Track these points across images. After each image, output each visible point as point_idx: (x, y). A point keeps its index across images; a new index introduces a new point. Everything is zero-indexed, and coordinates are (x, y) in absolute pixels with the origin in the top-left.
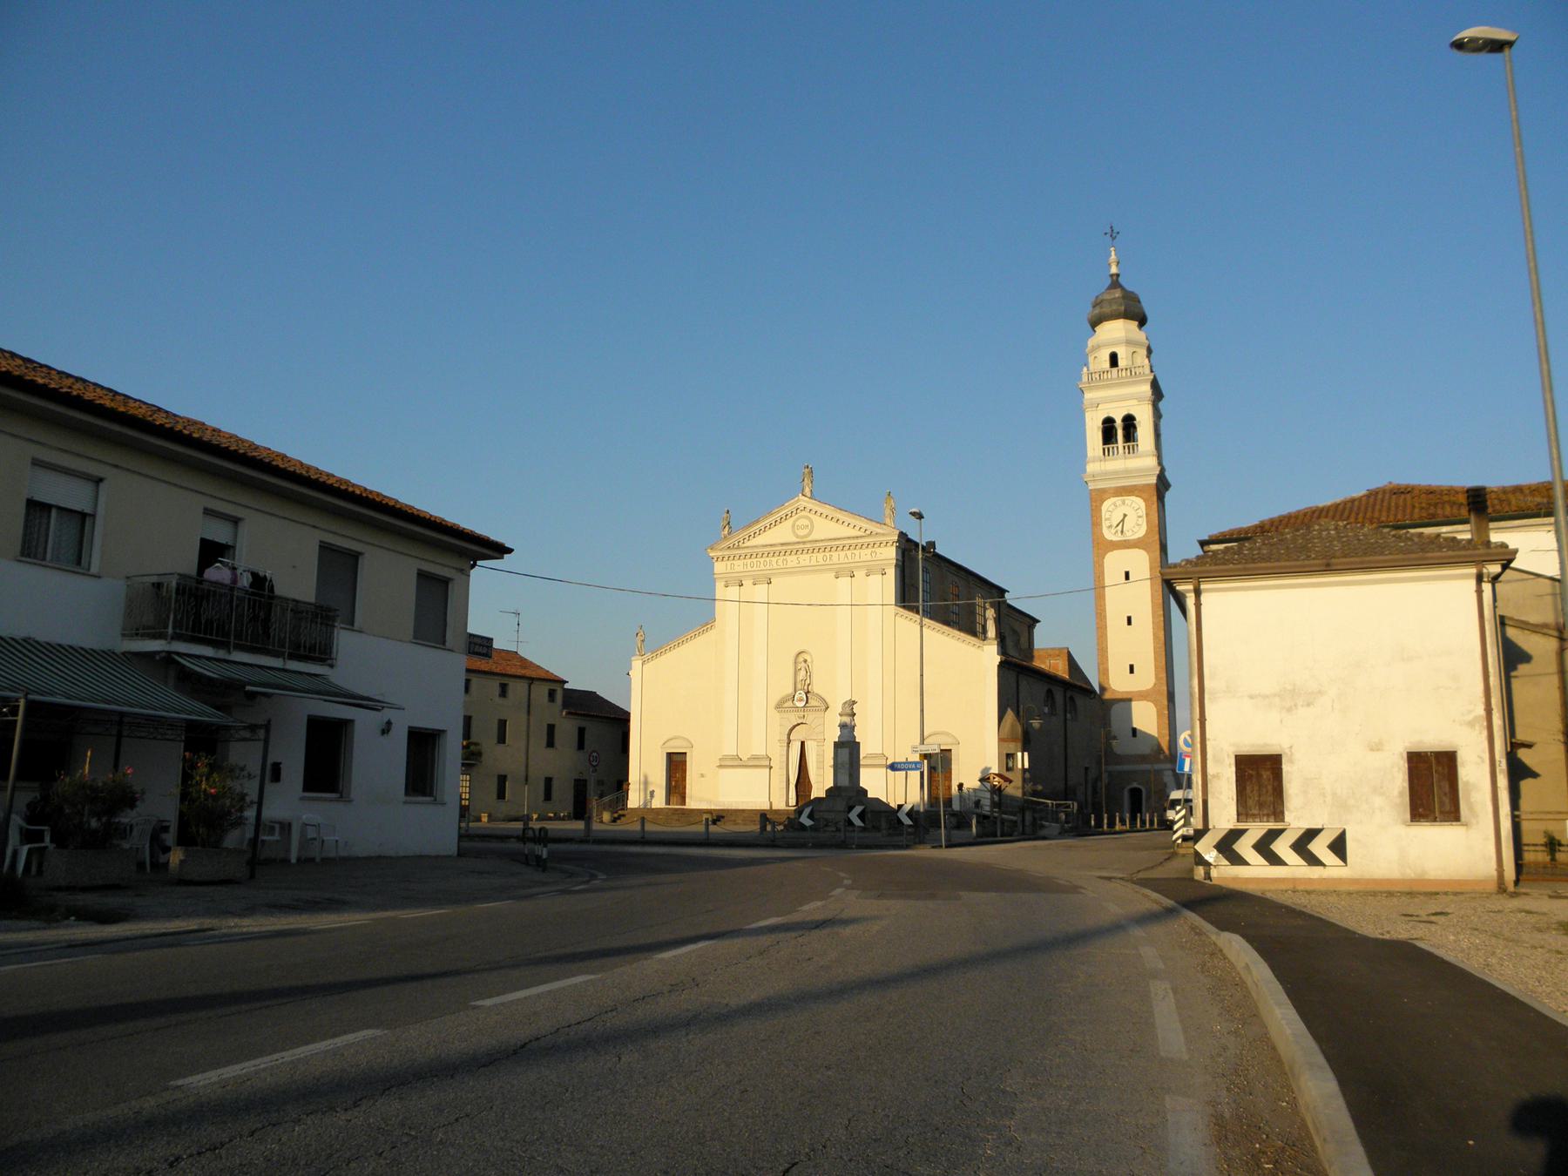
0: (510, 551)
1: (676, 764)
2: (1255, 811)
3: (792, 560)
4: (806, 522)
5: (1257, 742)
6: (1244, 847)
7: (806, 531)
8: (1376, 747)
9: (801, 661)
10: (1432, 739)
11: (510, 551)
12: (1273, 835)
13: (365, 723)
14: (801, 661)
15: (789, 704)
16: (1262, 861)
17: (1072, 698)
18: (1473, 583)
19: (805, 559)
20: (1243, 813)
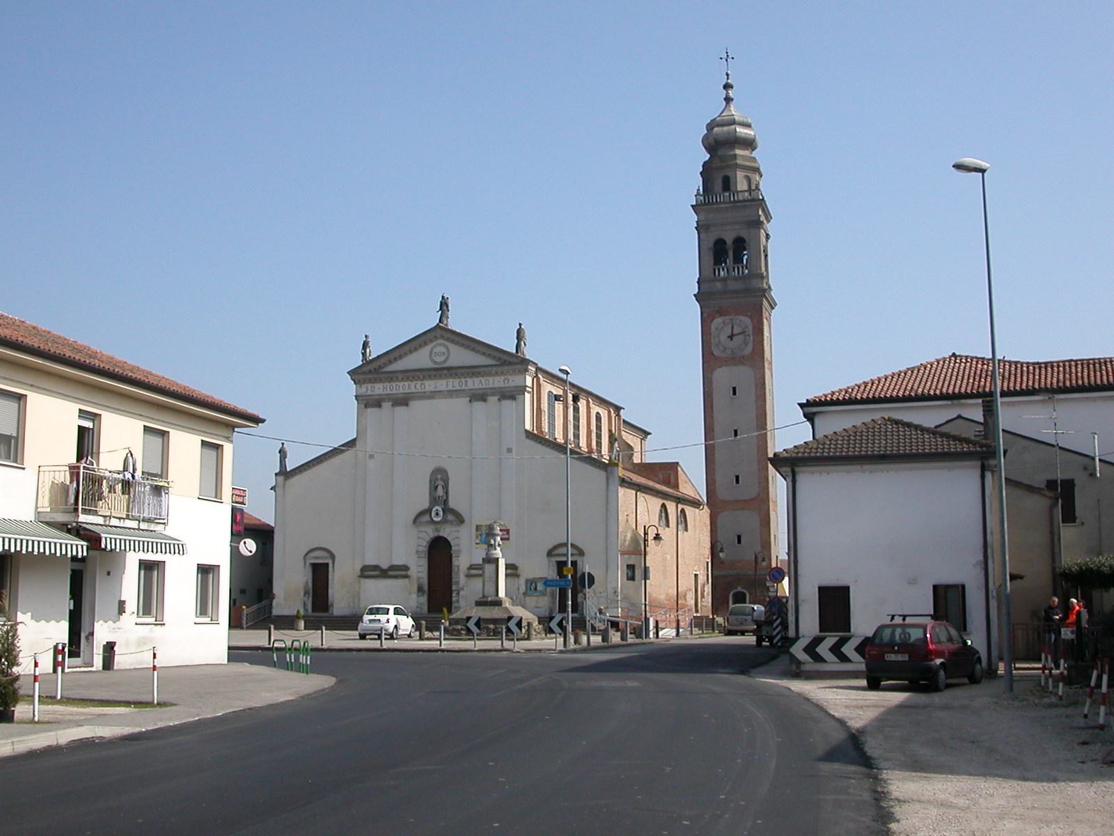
0: (263, 421)
1: (320, 573)
2: (1085, 362)
3: (430, 385)
4: (443, 349)
5: (831, 580)
6: (823, 649)
7: (443, 358)
8: (913, 582)
9: (439, 479)
10: (948, 577)
11: (263, 421)
12: (843, 641)
13: (171, 561)
14: (439, 479)
15: (426, 518)
16: (836, 659)
17: (683, 511)
18: (978, 472)
19: (442, 384)
20: (824, 626)
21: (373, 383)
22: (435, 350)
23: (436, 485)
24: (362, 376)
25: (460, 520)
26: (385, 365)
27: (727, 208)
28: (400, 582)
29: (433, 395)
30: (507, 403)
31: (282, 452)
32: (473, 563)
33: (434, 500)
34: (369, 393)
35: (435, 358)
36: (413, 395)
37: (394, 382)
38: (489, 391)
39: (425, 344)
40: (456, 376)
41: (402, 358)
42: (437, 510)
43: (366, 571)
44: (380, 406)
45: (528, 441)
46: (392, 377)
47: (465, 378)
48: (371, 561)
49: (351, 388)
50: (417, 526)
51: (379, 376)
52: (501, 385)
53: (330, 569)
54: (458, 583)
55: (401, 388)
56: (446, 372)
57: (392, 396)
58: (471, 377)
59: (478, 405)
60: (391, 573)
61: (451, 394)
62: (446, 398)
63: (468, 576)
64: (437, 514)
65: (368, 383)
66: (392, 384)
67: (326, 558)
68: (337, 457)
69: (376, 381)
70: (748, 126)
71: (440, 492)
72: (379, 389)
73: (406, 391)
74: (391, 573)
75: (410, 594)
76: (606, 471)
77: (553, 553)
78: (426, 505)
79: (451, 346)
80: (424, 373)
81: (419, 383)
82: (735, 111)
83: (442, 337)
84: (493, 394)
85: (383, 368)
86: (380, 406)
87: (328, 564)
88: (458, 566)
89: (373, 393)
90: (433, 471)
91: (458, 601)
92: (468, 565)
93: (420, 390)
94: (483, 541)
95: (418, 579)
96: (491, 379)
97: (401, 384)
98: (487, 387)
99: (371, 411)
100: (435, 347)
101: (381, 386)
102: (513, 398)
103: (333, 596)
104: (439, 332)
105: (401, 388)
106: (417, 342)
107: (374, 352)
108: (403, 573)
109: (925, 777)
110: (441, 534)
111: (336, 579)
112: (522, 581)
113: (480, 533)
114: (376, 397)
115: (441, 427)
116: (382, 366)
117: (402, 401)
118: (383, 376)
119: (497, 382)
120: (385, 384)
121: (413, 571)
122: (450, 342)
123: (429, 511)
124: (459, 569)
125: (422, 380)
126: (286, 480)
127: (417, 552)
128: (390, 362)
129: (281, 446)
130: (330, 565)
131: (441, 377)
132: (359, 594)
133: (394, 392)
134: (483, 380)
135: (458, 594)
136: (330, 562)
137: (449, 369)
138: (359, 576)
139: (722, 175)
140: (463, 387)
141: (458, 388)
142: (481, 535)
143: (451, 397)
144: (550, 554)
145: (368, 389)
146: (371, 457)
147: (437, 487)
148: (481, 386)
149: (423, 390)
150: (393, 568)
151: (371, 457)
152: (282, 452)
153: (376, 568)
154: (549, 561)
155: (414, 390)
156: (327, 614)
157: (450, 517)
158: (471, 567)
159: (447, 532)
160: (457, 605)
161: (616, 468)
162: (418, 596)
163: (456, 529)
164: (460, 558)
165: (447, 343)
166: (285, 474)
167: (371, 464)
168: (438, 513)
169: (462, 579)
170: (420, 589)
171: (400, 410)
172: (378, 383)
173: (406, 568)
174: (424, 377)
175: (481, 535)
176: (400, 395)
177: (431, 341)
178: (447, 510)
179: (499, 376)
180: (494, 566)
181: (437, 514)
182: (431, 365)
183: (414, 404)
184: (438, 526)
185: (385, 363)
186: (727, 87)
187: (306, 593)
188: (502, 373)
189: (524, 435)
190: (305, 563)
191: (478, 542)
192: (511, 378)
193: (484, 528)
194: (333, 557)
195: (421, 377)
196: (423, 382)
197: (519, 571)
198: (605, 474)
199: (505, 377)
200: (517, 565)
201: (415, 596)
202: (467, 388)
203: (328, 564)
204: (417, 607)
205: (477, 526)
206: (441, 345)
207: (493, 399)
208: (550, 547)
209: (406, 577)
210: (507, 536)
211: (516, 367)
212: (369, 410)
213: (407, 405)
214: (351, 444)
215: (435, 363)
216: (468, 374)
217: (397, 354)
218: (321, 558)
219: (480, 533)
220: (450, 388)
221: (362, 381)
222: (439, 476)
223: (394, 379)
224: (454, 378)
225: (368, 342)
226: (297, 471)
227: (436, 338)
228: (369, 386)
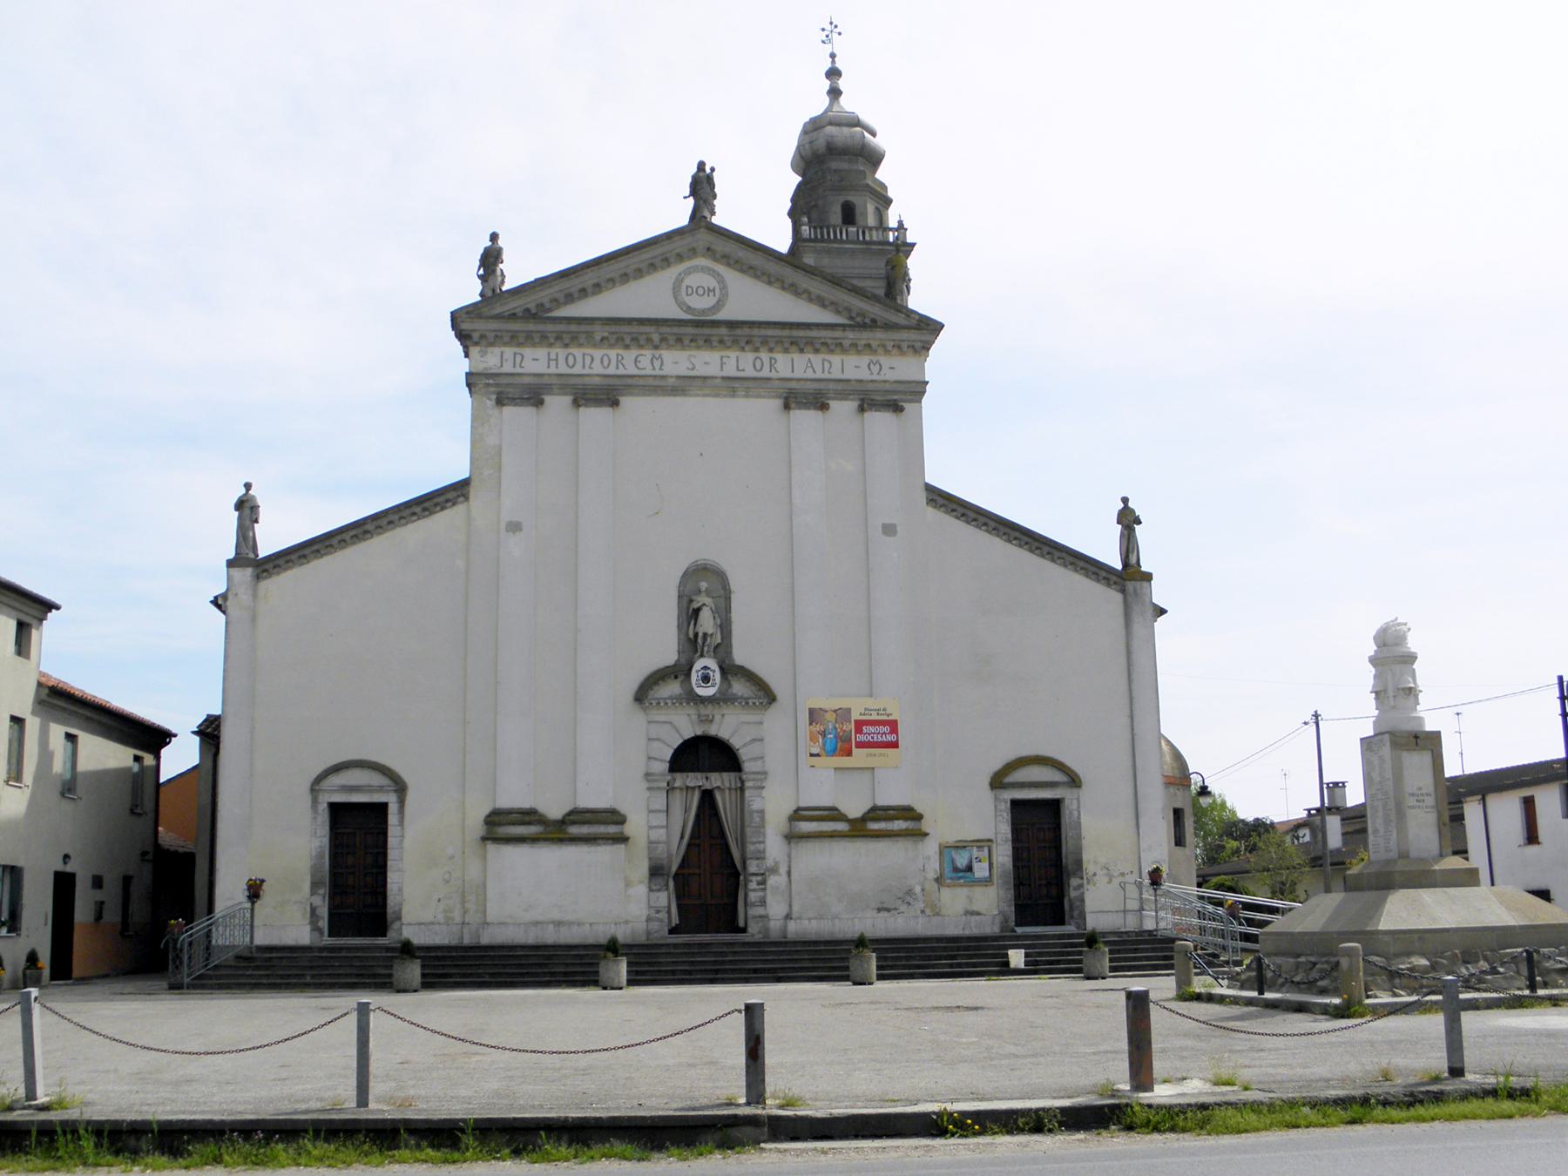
3: (676, 362)
4: (711, 282)
14: (703, 597)
15: (673, 688)
19: (708, 362)
21: (519, 345)
22: (687, 281)
23: (695, 605)
24: (493, 325)
25: (767, 695)
26: (556, 303)
27: (853, 251)
28: (603, 854)
29: (681, 386)
30: (879, 420)
31: (247, 508)
32: (802, 804)
33: (692, 645)
34: (508, 368)
35: (687, 299)
36: (630, 381)
37: (580, 345)
38: (831, 386)
39: (666, 262)
40: (749, 344)
41: (669, 265)
42: (705, 668)
43: (500, 824)
44: (539, 403)
45: (930, 510)
46: (580, 332)
47: (771, 350)
48: (513, 797)
49: (454, 361)
50: (645, 710)
51: (541, 327)
52: (864, 374)
53: (393, 819)
54: (761, 856)
55: (596, 362)
56: (723, 331)
57: (573, 381)
58: (786, 351)
59: (805, 419)
60: (574, 830)
61: (733, 386)
62: (717, 396)
63: (792, 837)
64: (706, 679)
65: (505, 344)
66: (575, 351)
67: (381, 789)
68: (411, 527)
69: (529, 340)
70: (874, 135)
71: (707, 623)
72: (535, 361)
73: (612, 370)
74: (574, 830)
75: (628, 884)
76: (1123, 591)
77: (1009, 779)
78: (669, 655)
79: (732, 277)
80: (665, 329)
81: (648, 353)
82: (847, 104)
83: (709, 251)
84: (843, 395)
85: (550, 310)
86: (539, 403)
87: (384, 806)
88: (762, 812)
89: (518, 370)
90: (685, 574)
91: (763, 902)
92: (789, 809)
93: (649, 371)
94: (829, 747)
95: (652, 844)
96: (836, 359)
97: (598, 353)
98: (826, 376)
99: (515, 415)
100: (688, 272)
101: (541, 353)
102: (896, 408)
103: (400, 890)
104: (703, 237)
105: (596, 362)
106: (647, 255)
107: (515, 274)
108: (612, 829)
109: (297, 1101)
110: (713, 730)
111: (407, 842)
112: (930, 848)
113: (819, 728)
114: (526, 380)
115: (706, 467)
116: (548, 305)
117: (606, 395)
118: (549, 327)
119: (853, 367)
120: (554, 351)
121: (636, 826)
122: (729, 265)
123: (680, 671)
124: (763, 819)
125: (656, 348)
126: (258, 578)
127: (647, 775)
128: (584, 293)
129: (243, 491)
130: (393, 809)
131: (708, 343)
132: (484, 886)
133: (577, 370)
134: (816, 359)
135: (763, 882)
136: (391, 799)
137: (732, 325)
138: (484, 839)
139: (842, 199)
140: (765, 373)
141: (750, 372)
142: (824, 734)
143: (733, 393)
144: (998, 782)
145: (494, 359)
146: (515, 527)
147: (697, 611)
148: (810, 374)
149: (658, 372)
150: (577, 816)
151: (515, 527)
152: (247, 508)
153: (529, 816)
154: (996, 799)
155: (632, 370)
156: (380, 941)
157: (739, 687)
158: (798, 815)
159: (729, 726)
160: (760, 911)
161: (1145, 584)
162: (651, 890)
163: (756, 718)
164: (764, 793)
165: (721, 269)
166: (245, 558)
167: (515, 546)
168: (706, 674)
169: (774, 847)
170: (656, 871)
171: (594, 416)
172: (534, 345)
173: (614, 817)
174: (663, 340)
175: (824, 734)
176: (597, 380)
177: (680, 258)
178: (729, 670)
179: (859, 352)
180: (1425, 758)
181: (706, 679)
182: (676, 313)
183: (631, 404)
184: (707, 710)
185: (556, 300)
186: (833, 73)
187: (315, 886)
188: (854, 345)
189: (922, 497)
190: (315, 802)
191: (815, 751)
192: (885, 361)
193: (830, 717)
194: (400, 788)
195: (656, 338)
196: (657, 353)
197: (926, 826)
198: (1119, 597)
199: (874, 359)
200: (919, 808)
201: (641, 890)
202: (773, 375)
203: (384, 806)
204: (649, 919)
205: (812, 712)
206: (704, 269)
207: (843, 409)
208: (997, 765)
209: (622, 839)
210: (890, 738)
211: (904, 335)
212: (509, 411)
213: (615, 403)
214: (456, 492)
215: (689, 309)
216: (780, 341)
217: (589, 279)
218: (362, 789)
219: (819, 728)
220: (730, 371)
221: (491, 335)
222: (704, 585)
223: (582, 339)
224: (743, 349)
225: (500, 250)
226: (293, 557)
227: (693, 252)
228: (509, 351)
